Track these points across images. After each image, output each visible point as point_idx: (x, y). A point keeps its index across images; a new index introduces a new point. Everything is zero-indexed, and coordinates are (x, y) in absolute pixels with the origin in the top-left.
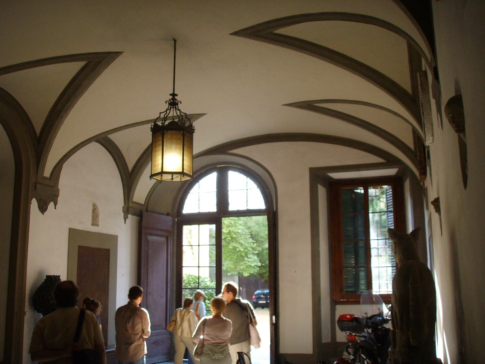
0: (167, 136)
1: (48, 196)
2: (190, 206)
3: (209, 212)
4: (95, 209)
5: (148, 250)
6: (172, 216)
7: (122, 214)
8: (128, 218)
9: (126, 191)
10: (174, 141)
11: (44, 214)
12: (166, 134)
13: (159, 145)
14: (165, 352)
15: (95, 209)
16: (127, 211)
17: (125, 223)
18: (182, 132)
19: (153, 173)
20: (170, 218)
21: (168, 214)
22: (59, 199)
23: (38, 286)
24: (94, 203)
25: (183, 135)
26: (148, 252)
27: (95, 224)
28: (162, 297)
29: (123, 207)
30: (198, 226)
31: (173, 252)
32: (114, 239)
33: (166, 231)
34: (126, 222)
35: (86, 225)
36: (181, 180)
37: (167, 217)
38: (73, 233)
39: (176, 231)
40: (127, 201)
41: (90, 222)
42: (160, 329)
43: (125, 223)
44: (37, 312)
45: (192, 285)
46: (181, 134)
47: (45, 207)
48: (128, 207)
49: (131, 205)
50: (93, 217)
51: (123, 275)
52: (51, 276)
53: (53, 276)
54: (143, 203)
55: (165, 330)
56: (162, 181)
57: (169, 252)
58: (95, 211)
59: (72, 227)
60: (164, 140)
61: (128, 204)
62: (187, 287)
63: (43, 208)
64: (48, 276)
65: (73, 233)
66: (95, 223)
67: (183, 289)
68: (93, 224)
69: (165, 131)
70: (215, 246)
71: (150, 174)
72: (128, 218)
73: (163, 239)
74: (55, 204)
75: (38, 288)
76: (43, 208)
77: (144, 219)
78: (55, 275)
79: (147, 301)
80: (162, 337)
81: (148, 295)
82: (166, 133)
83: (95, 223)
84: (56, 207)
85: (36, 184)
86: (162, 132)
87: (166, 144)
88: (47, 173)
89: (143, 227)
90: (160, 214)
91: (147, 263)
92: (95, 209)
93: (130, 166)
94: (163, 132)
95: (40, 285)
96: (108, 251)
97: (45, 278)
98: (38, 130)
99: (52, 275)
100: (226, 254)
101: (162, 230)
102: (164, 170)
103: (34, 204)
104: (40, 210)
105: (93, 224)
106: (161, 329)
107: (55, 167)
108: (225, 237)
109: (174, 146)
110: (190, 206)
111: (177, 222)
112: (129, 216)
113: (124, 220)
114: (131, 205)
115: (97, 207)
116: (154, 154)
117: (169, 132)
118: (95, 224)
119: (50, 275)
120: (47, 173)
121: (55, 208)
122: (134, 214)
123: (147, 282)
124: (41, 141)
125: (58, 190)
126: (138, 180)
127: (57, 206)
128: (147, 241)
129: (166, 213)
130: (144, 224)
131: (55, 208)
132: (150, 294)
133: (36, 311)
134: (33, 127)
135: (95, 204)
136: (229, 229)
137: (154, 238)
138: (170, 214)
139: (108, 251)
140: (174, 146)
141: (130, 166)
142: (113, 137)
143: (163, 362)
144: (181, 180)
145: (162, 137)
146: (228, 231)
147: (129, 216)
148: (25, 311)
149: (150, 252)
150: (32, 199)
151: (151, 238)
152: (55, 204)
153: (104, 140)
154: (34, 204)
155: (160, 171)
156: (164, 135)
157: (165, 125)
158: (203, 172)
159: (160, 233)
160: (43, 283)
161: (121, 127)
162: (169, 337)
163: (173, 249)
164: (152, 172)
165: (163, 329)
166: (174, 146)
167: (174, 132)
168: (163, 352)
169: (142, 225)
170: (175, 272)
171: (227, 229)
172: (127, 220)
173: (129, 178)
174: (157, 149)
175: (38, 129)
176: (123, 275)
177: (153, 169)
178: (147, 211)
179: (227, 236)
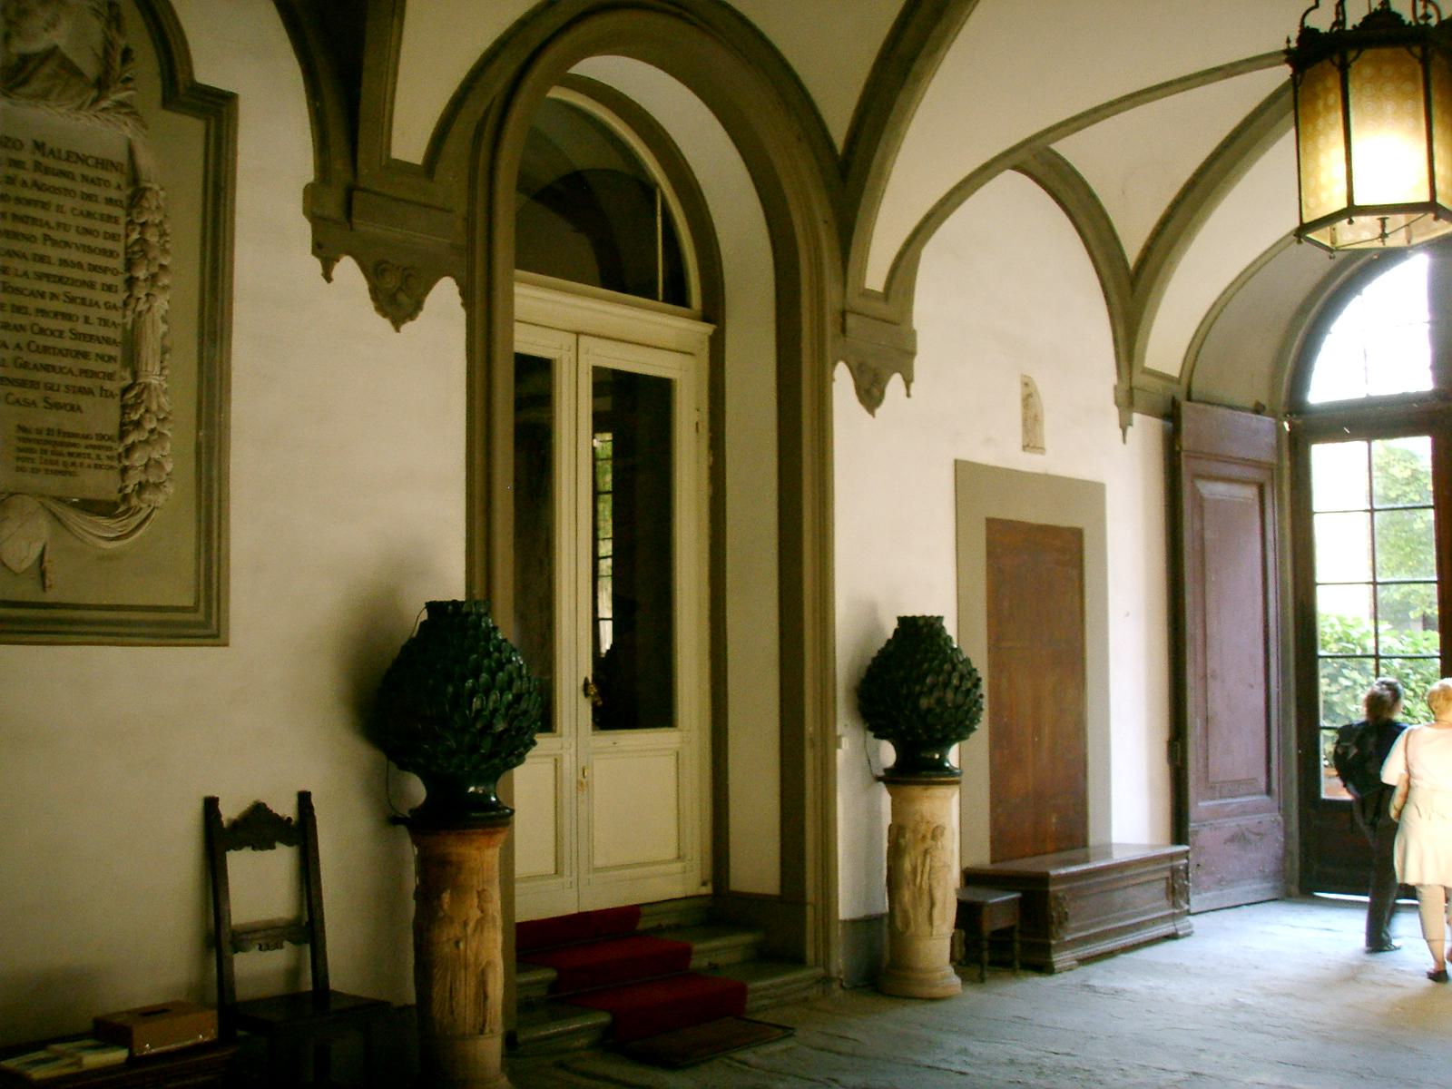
0: (1361, 71)
1: (884, 360)
2: (1330, 383)
3: (1403, 393)
4: (1029, 399)
5: (1203, 529)
6: (1274, 414)
7: (1115, 410)
8: (1131, 425)
9: (1121, 333)
10: (1389, 88)
11: (874, 416)
12: (1353, 65)
13: (1328, 108)
14: (1267, 870)
15: (1029, 399)
16: (1128, 400)
17: (1124, 441)
18: (1417, 50)
19: (1306, 220)
20: (1266, 422)
21: (1258, 409)
22: (919, 364)
23: (874, 654)
24: (1025, 376)
25: (1425, 62)
26: (1202, 538)
27: (1031, 445)
28: (1252, 686)
29: (1116, 388)
30: (1364, 444)
31: (1282, 535)
32: (1092, 493)
33: (1257, 464)
34: (1128, 438)
35: (1005, 453)
36: (1409, 242)
37: (1259, 417)
38: (967, 477)
39: (1287, 463)
40: (1124, 364)
41: (1017, 439)
42: (1248, 794)
43: (1124, 441)
44: (875, 737)
45: (1330, 646)
46: (1414, 56)
47: (875, 392)
48: (1131, 388)
49: (1139, 379)
50: (1025, 421)
51: (1128, 615)
52: (914, 618)
53: (920, 618)
54: (1175, 373)
55: (1265, 797)
56: (1337, 250)
57: (1270, 536)
58: (1031, 400)
59: (963, 456)
60: (1350, 86)
61: (1130, 379)
62: (1352, 654)
63: (870, 396)
64: (905, 617)
65: (967, 477)
66: (1032, 443)
67: (1438, 654)
68: (1025, 444)
69: (1352, 55)
70: (1431, 512)
71: (1297, 224)
72: (1131, 425)
73: (1250, 493)
74: (908, 381)
75: (874, 660)
76: (870, 396)
77: (1186, 426)
78: (928, 614)
79: (1206, 701)
80: (1257, 821)
81: (1209, 680)
82: (1355, 59)
83: (1032, 443)
84: (912, 392)
85: (843, 314)
86: (1336, 59)
87: (1360, 99)
88: (875, 278)
89: (1182, 454)
90: (1231, 407)
91: (1202, 580)
92: (1030, 395)
93: (1132, 253)
94: (1343, 57)
95: (879, 648)
96: (1078, 534)
97: (894, 625)
98: (839, 131)
99: (918, 614)
100: (1403, 549)
101: (1245, 462)
102: (1358, 202)
103: (842, 382)
104: (862, 400)
105: (1028, 446)
106: (1254, 794)
107: (900, 256)
108: (1400, 492)
109: (1389, 108)
110: (1330, 383)
111: (1290, 433)
112: (1137, 417)
113: (1120, 432)
114: (1139, 379)
115: (1036, 390)
116: (1304, 149)
117: (1368, 54)
118: (1031, 445)
119: (909, 614)
120: (875, 278)
121: (908, 395)
122: (1149, 412)
123: (1205, 635)
124: (850, 173)
125: (913, 334)
126: (1161, 292)
127: (913, 386)
128: (1200, 501)
129: (1251, 404)
130: (1186, 442)
131: (908, 395)
132: (1214, 677)
133: (871, 735)
134: (819, 120)
135: (1030, 377)
136: (1414, 467)
137: (1220, 489)
138: (1264, 407)
139: (1078, 534)
140: (1389, 107)
141: (1132, 253)
142: (1068, 148)
143: (1261, 902)
144: (1409, 242)
145: (1338, 75)
146: (1407, 473)
147: (1137, 417)
148: (838, 733)
149: (1209, 535)
150: (834, 364)
151: (1214, 490)
152: (908, 381)
153: (1040, 162)
154: (842, 382)
155: (1341, 204)
156: (1349, 66)
157: (1349, 27)
158: (1376, 257)
159: (1235, 471)
160: (889, 642)
161: (1111, 104)
162: (1280, 818)
163: (1281, 528)
164: (1304, 216)
165: (1261, 793)
166: (1389, 107)
167: (1386, 52)
168: (1261, 868)
169: (1181, 447)
170: (1290, 599)
171: (1406, 467)
172: (1130, 429)
173: (1129, 288)
174: (1321, 123)
175: (838, 126)
176: (1128, 615)
177: (1309, 201)
178: (1189, 399)
179: (1407, 489)
